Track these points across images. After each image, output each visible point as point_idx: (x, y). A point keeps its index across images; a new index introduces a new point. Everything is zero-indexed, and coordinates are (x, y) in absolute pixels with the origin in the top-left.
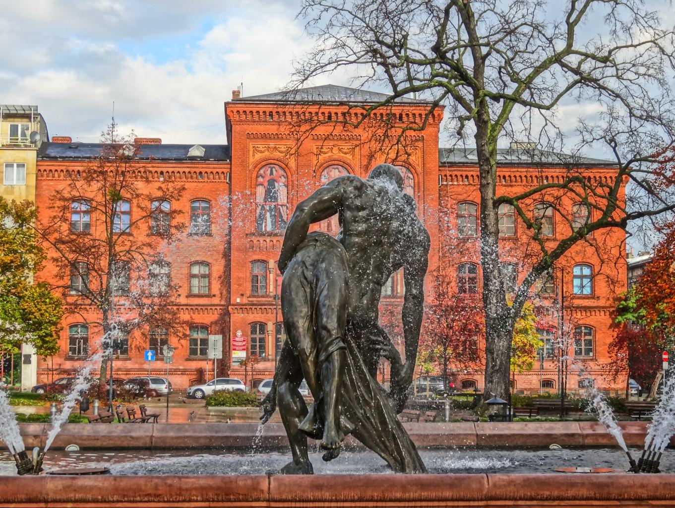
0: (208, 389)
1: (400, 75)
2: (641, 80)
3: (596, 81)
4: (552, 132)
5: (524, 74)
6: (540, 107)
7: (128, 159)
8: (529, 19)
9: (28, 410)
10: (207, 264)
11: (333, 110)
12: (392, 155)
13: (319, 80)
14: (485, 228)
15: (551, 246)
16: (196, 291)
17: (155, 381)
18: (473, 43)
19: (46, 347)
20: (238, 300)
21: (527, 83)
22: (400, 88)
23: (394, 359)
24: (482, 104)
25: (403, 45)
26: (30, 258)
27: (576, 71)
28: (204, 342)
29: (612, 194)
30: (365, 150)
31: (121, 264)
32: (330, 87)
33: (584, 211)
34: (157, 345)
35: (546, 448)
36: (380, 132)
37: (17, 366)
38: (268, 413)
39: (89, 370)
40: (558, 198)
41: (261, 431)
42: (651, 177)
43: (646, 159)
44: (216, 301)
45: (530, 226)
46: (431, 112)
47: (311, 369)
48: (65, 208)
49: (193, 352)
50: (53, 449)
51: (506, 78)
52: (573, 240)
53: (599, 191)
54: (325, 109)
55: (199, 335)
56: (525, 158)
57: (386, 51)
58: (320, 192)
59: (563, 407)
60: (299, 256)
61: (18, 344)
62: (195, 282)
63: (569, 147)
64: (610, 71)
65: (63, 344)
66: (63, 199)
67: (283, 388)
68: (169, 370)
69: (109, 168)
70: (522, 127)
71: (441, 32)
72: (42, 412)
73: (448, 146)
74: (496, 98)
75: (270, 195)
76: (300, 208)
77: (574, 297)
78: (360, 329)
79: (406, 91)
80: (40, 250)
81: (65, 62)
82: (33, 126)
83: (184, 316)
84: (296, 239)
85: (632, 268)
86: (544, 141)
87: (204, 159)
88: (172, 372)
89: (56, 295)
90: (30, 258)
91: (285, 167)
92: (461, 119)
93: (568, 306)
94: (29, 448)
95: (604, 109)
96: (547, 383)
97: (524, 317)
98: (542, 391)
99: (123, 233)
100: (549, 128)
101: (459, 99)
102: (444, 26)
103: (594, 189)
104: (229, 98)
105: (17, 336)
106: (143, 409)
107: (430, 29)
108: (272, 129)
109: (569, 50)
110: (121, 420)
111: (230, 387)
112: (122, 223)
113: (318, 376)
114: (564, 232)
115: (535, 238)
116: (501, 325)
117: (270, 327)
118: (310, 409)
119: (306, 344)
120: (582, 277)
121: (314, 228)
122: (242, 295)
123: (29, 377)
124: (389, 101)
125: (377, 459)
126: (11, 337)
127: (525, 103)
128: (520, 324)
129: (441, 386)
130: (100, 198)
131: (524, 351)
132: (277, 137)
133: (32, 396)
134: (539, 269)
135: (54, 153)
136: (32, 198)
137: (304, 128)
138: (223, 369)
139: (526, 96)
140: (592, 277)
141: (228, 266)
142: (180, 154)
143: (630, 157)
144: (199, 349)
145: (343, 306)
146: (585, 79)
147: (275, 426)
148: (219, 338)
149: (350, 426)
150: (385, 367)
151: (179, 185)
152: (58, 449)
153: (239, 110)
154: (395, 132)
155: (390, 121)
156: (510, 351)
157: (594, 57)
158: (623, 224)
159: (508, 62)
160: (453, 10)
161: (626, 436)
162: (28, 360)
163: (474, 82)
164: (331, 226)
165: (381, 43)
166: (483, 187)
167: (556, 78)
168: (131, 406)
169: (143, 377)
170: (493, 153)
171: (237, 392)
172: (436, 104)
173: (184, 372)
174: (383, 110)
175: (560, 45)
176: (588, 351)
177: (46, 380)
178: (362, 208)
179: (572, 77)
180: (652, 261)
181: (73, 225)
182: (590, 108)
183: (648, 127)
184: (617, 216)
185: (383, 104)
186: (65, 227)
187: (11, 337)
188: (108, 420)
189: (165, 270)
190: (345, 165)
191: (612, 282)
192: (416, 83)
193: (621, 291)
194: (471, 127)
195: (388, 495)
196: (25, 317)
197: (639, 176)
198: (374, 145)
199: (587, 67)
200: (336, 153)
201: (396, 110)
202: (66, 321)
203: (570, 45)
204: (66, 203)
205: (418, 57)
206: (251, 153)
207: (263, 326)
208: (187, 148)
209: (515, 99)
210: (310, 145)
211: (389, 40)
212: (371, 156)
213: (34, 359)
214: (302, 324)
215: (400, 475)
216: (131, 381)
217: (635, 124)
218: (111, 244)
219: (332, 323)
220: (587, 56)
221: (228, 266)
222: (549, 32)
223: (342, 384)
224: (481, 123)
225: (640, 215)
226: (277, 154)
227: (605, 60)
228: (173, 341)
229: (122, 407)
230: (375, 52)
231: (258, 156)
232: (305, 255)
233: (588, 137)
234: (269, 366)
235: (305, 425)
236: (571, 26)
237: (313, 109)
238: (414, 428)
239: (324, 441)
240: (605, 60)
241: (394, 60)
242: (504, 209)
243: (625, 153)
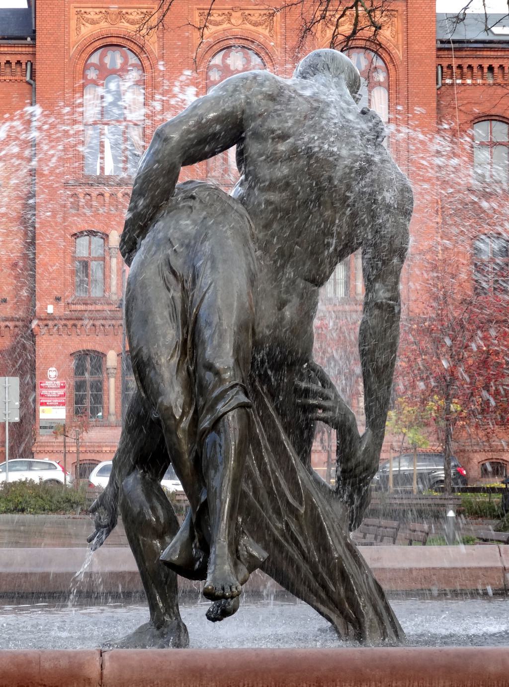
20: (50, 309)
23: (344, 429)
47: (185, 447)
78: (279, 370)
111: (36, 476)
122: (58, 299)
145: (247, 327)
147: (118, 557)
149: (259, 553)
164: (223, 171)
206: (73, 23)
207: (99, 357)
226: (125, 27)
231: (87, 30)
234: (107, 437)
238: (384, 557)
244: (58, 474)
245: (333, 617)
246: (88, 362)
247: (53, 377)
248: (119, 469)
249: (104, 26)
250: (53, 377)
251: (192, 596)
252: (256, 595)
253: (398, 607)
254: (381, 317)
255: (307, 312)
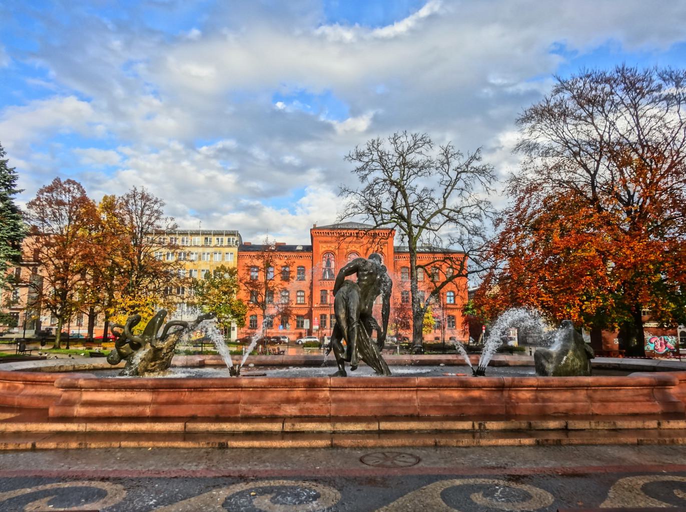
0: (304, 340)
1: (379, 218)
2: (473, 220)
3: (455, 220)
4: (438, 240)
5: (427, 218)
6: (433, 230)
7: (273, 251)
8: (428, 196)
9: (234, 349)
10: (303, 292)
11: (352, 231)
12: (376, 249)
13: (344, 221)
14: (412, 276)
15: (438, 284)
16: (299, 302)
17: (283, 337)
18: (407, 206)
19: (241, 324)
21: (428, 221)
22: (379, 223)
23: (378, 330)
24: (411, 229)
25: (380, 207)
26: (235, 289)
27: (447, 216)
28: (303, 322)
29: (462, 265)
30: (365, 247)
31: (270, 293)
32: (351, 223)
33: (451, 271)
34: (284, 323)
35: (438, 365)
36: (371, 240)
37: (230, 331)
38: (329, 351)
39: (259, 334)
40: (441, 266)
41: (326, 359)
42: (477, 257)
43: (475, 250)
44: (307, 306)
45: (430, 277)
46: (391, 232)
47: (346, 334)
48: (248, 270)
49: (298, 326)
50: (244, 366)
51: (420, 219)
52: (447, 282)
53: (457, 263)
54: (350, 231)
55: (301, 320)
56: (427, 250)
57: (373, 209)
58: (349, 264)
59: (442, 348)
60: (342, 289)
61: (230, 323)
62: (299, 298)
63: (445, 245)
64: (460, 216)
65: (247, 323)
66: (248, 266)
67: (335, 341)
68: (289, 332)
69: (265, 254)
70: (426, 237)
71: (394, 202)
72: (239, 350)
73: (398, 245)
74: (416, 227)
75: (328, 264)
76: (341, 270)
77: (447, 304)
78: (365, 317)
79: (381, 224)
80: (239, 286)
81: (240, 209)
82: (236, 238)
83: (294, 312)
84: (340, 283)
85: (470, 293)
86: (435, 243)
87: (302, 251)
88: (290, 334)
89: (245, 303)
90: (235, 289)
91: (334, 254)
92: (402, 235)
93: (445, 308)
94: (235, 365)
95: (459, 231)
96: (437, 338)
97: (428, 312)
98: (435, 342)
99: (271, 280)
100: (437, 238)
101: (402, 227)
102: (396, 199)
103: (454, 262)
104: (312, 227)
105: (229, 320)
106: (278, 349)
107: (390, 200)
108: (329, 239)
109: (444, 208)
110: (270, 353)
111: (312, 340)
112: (270, 276)
113: (348, 336)
114: (443, 278)
115: (432, 281)
116: (419, 315)
117: (328, 316)
118: (345, 349)
119: (344, 324)
120: (450, 296)
121: (346, 278)
123: (234, 336)
124: (375, 228)
125: (371, 370)
126: (227, 320)
127: (427, 229)
128: (426, 315)
129: (395, 339)
130: (262, 266)
131: (428, 326)
132: (331, 242)
133: (235, 343)
134: (433, 293)
135: (245, 248)
136: (236, 266)
137: (341, 238)
138: (310, 333)
139: (428, 226)
140: (455, 297)
141: (311, 293)
142: (291, 249)
143: (469, 249)
144: (300, 325)
145: (359, 309)
146: (451, 219)
147: (332, 356)
148: (308, 320)
149: (361, 357)
150: (375, 333)
151: (292, 261)
152: (246, 365)
153: (316, 232)
154: (377, 240)
155: (375, 236)
156: (422, 326)
157: (454, 211)
158: (466, 276)
159: (421, 213)
160: (399, 193)
161: (471, 360)
162: (234, 329)
163: (407, 220)
164: (353, 278)
165: (371, 206)
166: (411, 262)
167: (439, 219)
168: (274, 347)
169: (278, 335)
170: (415, 248)
171: (315, 342)
172: (392, 229)
173: (294, 334)
174: (372, 232)
175: (441, 206)
176: (453, 325)
177: (241, 337)
178: (366, 271)
179: (446, 219)
180: (478, 290)
181: (251, 277)
182: (450, 228)
183: (476, 238)
184: (464, 272)
185: (371, 229)
186: (248, 277)
187: (227, 320)
188: (265, 353)
189: (287, 294)
190: (357, 253)
191: (462, 298)
192: (385, 221)
193: (466, 302)
194: (406, 239)
195: (377, 386)
196: (233, 312)
197: (473, 257)
198: (369, 245)
199: (451, 214)
200: (353, 248)
201: (377, 232)
202: (249, 313)
203: (444, 206)
204: (250, 268)
205: (386, 211)
207: (325, 315)
208: (296, 246)
209: (424, 227)
210: (344, 245)
211: (374, 205)
212: (368, 249)
213: (236, 329)
214: (342, 316)
215: (380, 377)
216: (273, 338)
217: (471, 237)
218: (266, 283)
219: (354, 316)
220: (451, 210)
221: (311, 293)
222: (436, 201)
223: (358, 340)
224: (410, 235)
225: (473, 272)
226: (331, 249)
227: (458, 212)
228: (290, 321)
229: (270, 348)
230: (369, 209)
231: (324, 249)
232: (344, 289)
233: (452, 242)
234: (328, 331)
235: (343, 356)
236: (445, 199)
237: (345, 231)
238: (387, 356)
239: (351, 363)
240: (458, 212)
241: (376, 212)
242: (420, 270)
243: (467, 248)
244: (317, 340)
245: (395, 378)
246: (323, 317)
247: (316, 319)
248: (332, 339)
249: (327, 249)
250: (316, 319)
251: (348, 365)
252: (361, 365)
253: (390, 368)
254: (386, 308)
255: (371, 306)
